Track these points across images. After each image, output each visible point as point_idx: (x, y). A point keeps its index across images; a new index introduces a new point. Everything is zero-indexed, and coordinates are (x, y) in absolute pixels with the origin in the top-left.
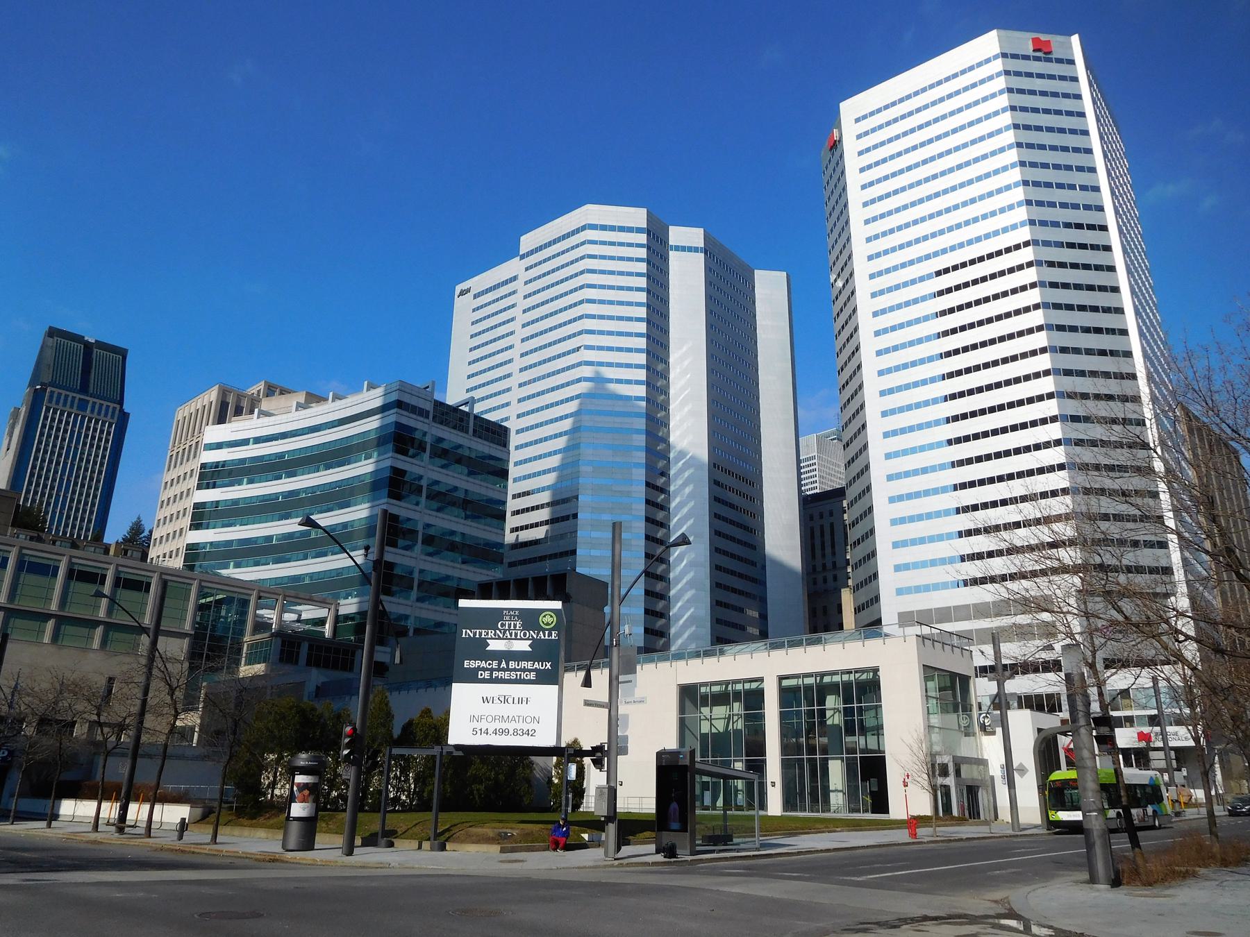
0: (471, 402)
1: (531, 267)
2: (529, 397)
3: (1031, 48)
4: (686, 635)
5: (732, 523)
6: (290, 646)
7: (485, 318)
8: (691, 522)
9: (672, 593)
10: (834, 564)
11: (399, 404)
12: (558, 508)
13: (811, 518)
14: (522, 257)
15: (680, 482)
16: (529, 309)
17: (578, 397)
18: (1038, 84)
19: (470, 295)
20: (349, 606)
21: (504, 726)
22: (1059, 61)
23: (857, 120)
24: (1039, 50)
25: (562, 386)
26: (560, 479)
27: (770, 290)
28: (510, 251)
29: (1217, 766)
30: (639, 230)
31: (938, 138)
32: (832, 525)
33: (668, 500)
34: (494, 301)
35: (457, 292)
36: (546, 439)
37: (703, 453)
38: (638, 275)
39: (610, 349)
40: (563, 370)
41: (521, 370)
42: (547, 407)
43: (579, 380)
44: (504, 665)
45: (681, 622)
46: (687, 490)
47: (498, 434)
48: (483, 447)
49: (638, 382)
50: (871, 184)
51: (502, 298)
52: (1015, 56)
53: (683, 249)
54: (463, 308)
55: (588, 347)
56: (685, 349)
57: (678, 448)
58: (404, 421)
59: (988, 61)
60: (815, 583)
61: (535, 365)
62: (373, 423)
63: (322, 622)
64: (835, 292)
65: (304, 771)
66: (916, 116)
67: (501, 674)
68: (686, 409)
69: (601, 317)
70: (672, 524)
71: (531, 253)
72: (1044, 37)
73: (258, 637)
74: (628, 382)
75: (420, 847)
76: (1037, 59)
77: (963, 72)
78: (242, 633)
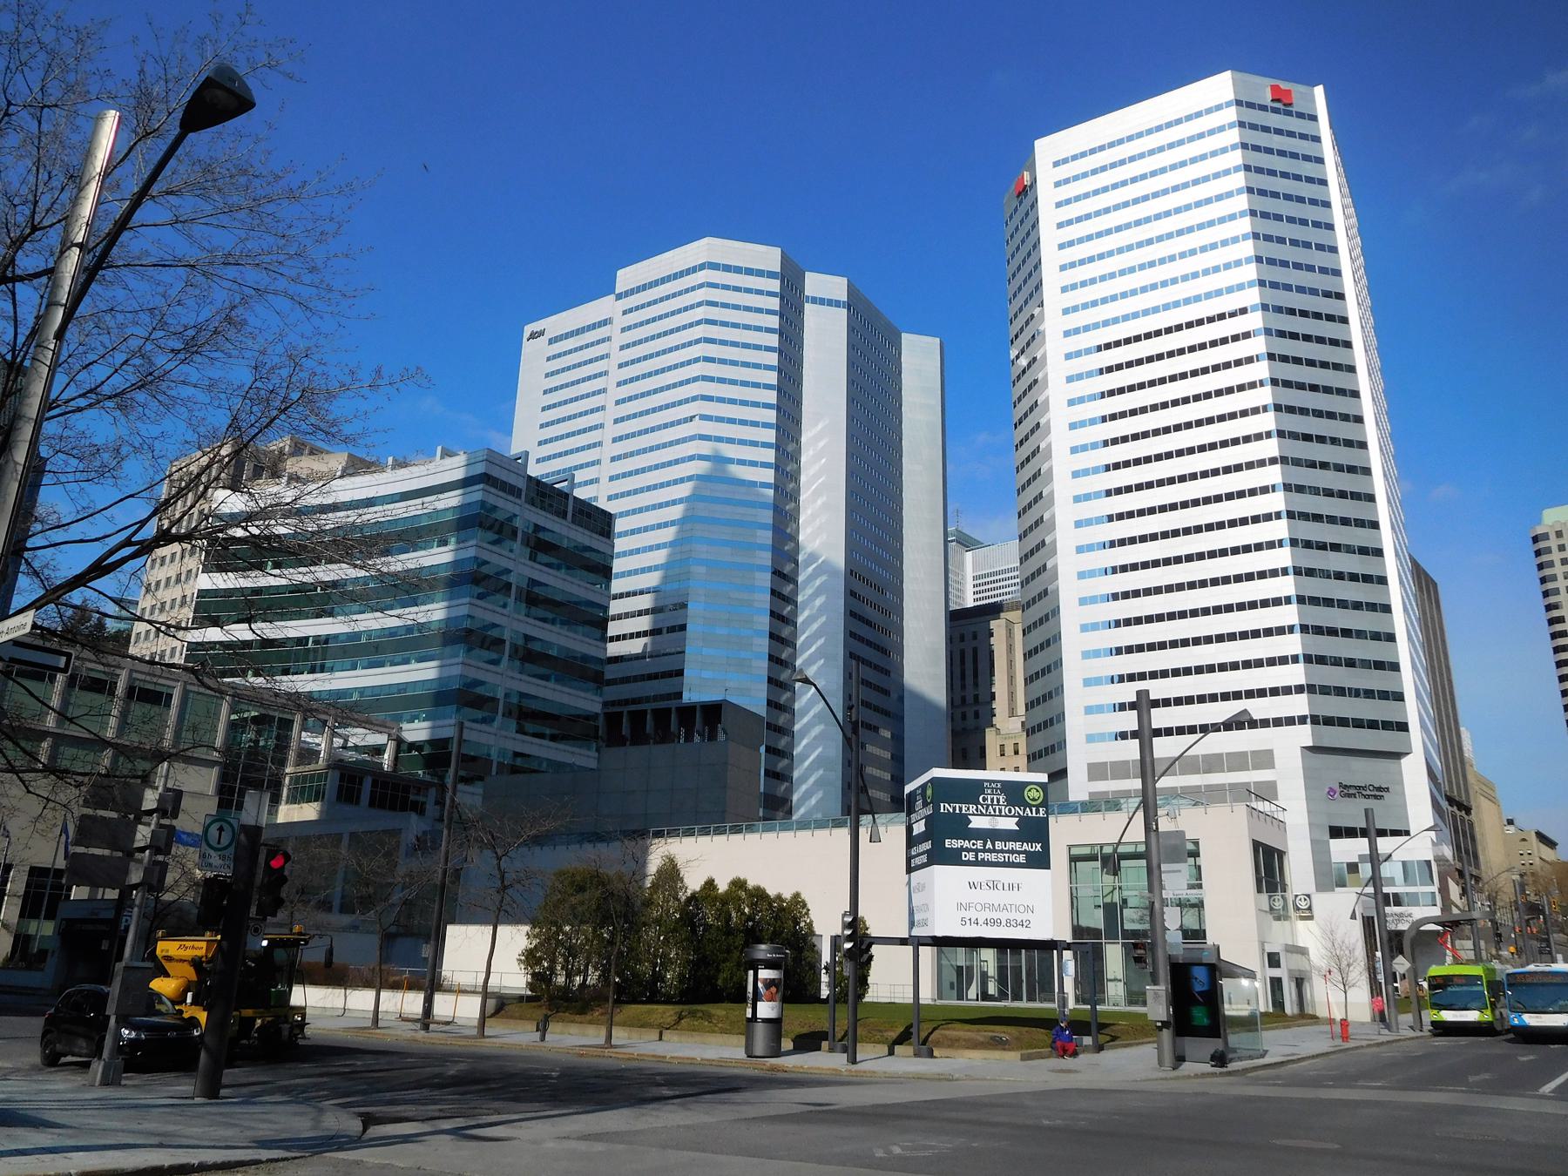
0: (568, 476)
1: (631, 310)
2: (624, 475)
3: (1269, 97)
4: (812, 780)
5: (869, 643)
6: (350, 782)
7: (563, 370)
8: (821, 641)
9: (797, 727)
10: (976, 697)
11: (485, 478)
12: (661, 615)
13: (962, 638)
14: (619, 297)
15: (809, 591)
16: (627, 364)
17: (690, 478)
18: (1277, 142)
19: (543, 340)
20: (417, 731)
21: (995, 915)
22: (1301, 115)
23: (1056, 164)
24: (1278, 100)
25: (669, 464)
26: (665, 579)
27: (919, 359)
28: (606, 287)
29: (107, 852)
30: (771, 275)
31: (1156, 195)
32: (975, 650)
33: (795, 613)
34: (576, 350)
35: (527, 334)
36: (646, 529)
37: (839, 559)
38: (769, 330)
39: (732, 421)
40: (671, 444)
41: (614, 440)
42: (649, 488)
43: (691, 458)
44: (989, 845)
45: (807, 764)
46: (818, 602)
47: (601, 523)
48: (582, 536)
49: (765, 465)
50: (1071, 244)
51: (587, 346)
52: (1250, 105)
53: (822, 301)
54: (534, 357)
55: (704, 417)
56: (820, 426)
57: (809, 550)
58: (492, 500)
59: (1219, 108)
60: (964, 717)
61: (633, 435)
62: (452, 500)
63: (378, 750)
64: (1015, 372)
65: (769, 965)
66: (1128, 166)
67: (987, 856)
68: (819, 502)
69: (722, 381)
70: (799, 642)
71: (627, 294)
72: (1284, 85)
73: (301, 769)
74: (753, 464)
75: (891, 1053)
76: (1275, 111)
77: (1189, 118)
78: (282, 763)
